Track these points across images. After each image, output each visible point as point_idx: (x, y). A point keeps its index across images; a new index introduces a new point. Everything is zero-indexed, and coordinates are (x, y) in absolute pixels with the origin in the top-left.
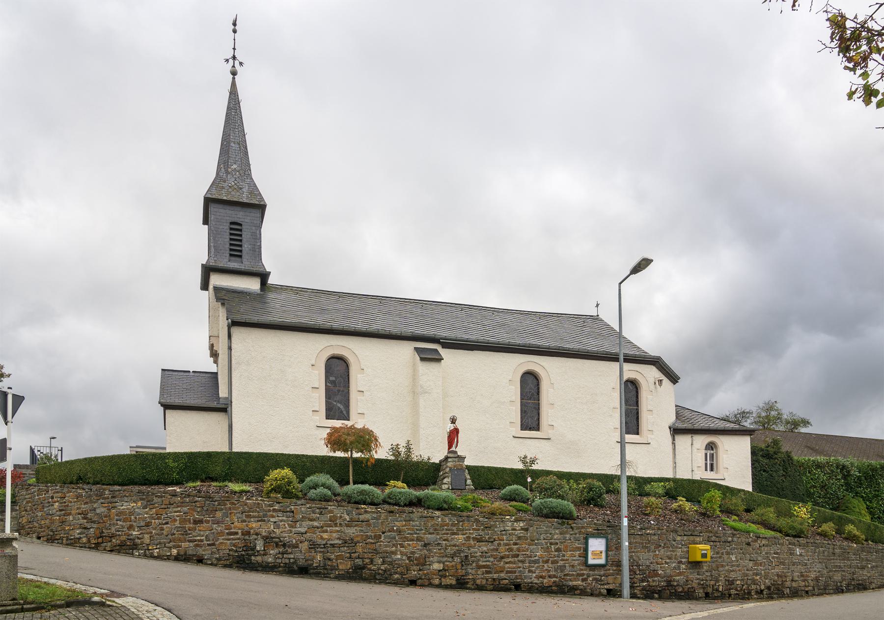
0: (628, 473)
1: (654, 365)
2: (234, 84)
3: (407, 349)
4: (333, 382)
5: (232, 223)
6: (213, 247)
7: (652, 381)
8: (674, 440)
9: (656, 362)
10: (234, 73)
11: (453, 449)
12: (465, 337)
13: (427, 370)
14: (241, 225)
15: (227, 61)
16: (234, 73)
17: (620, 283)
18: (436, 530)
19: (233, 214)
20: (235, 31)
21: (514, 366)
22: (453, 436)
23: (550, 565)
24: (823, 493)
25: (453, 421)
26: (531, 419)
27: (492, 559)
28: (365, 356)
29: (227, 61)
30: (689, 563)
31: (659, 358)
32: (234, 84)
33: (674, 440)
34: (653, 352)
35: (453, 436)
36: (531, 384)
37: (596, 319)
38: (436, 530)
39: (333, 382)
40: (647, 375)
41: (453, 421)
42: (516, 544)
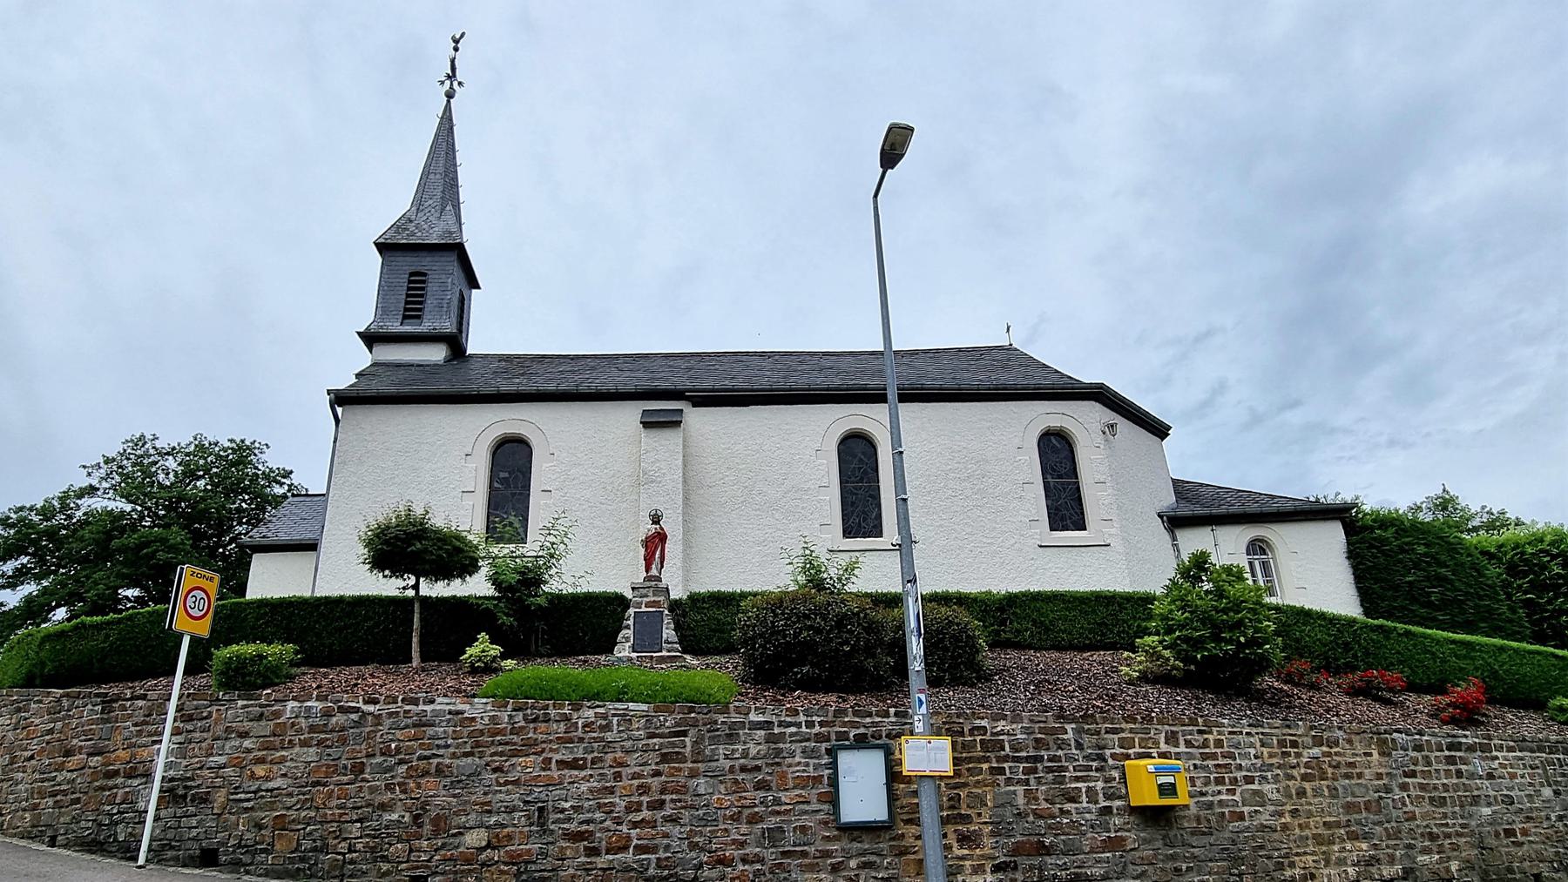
0: (926, 587)
1: (1096, 400)
2: (448, 108)
3: (631, 413)
4: (504, 481)
5: (412, 274)
6: (383, 309)
7: (1097, 427)
8: (1174, 539)
9: (1100, 395)
10: (450, 95)
11: (654, 572)
12: (728, 383)
13: (668, 440)
14: (425, 275)
15: (442, 83)
16: (450, 95)
17: (876, 196)
18: (478, 744)
19: (425, 266)
20: (456, 49)
21: (823, 427)
22: (655, 544)
23: (744, 828)
24: (1460, 611)
25: (656, 519)
26: (860, 514)
27: (598, 815)
28: (542, 426)
29: (442, 83)
30: (1134, 810)
31: (1101, 386)
32: (448, 108)
33: (1174, 539)
34: (1087, 376)
35: (655, 544)
36: (857, 456)
37: (1009, 349)
38: (478, 744)
39: (504, 481)
40: (1084, 421)
41: (656, 519)
42: (657, 774)
